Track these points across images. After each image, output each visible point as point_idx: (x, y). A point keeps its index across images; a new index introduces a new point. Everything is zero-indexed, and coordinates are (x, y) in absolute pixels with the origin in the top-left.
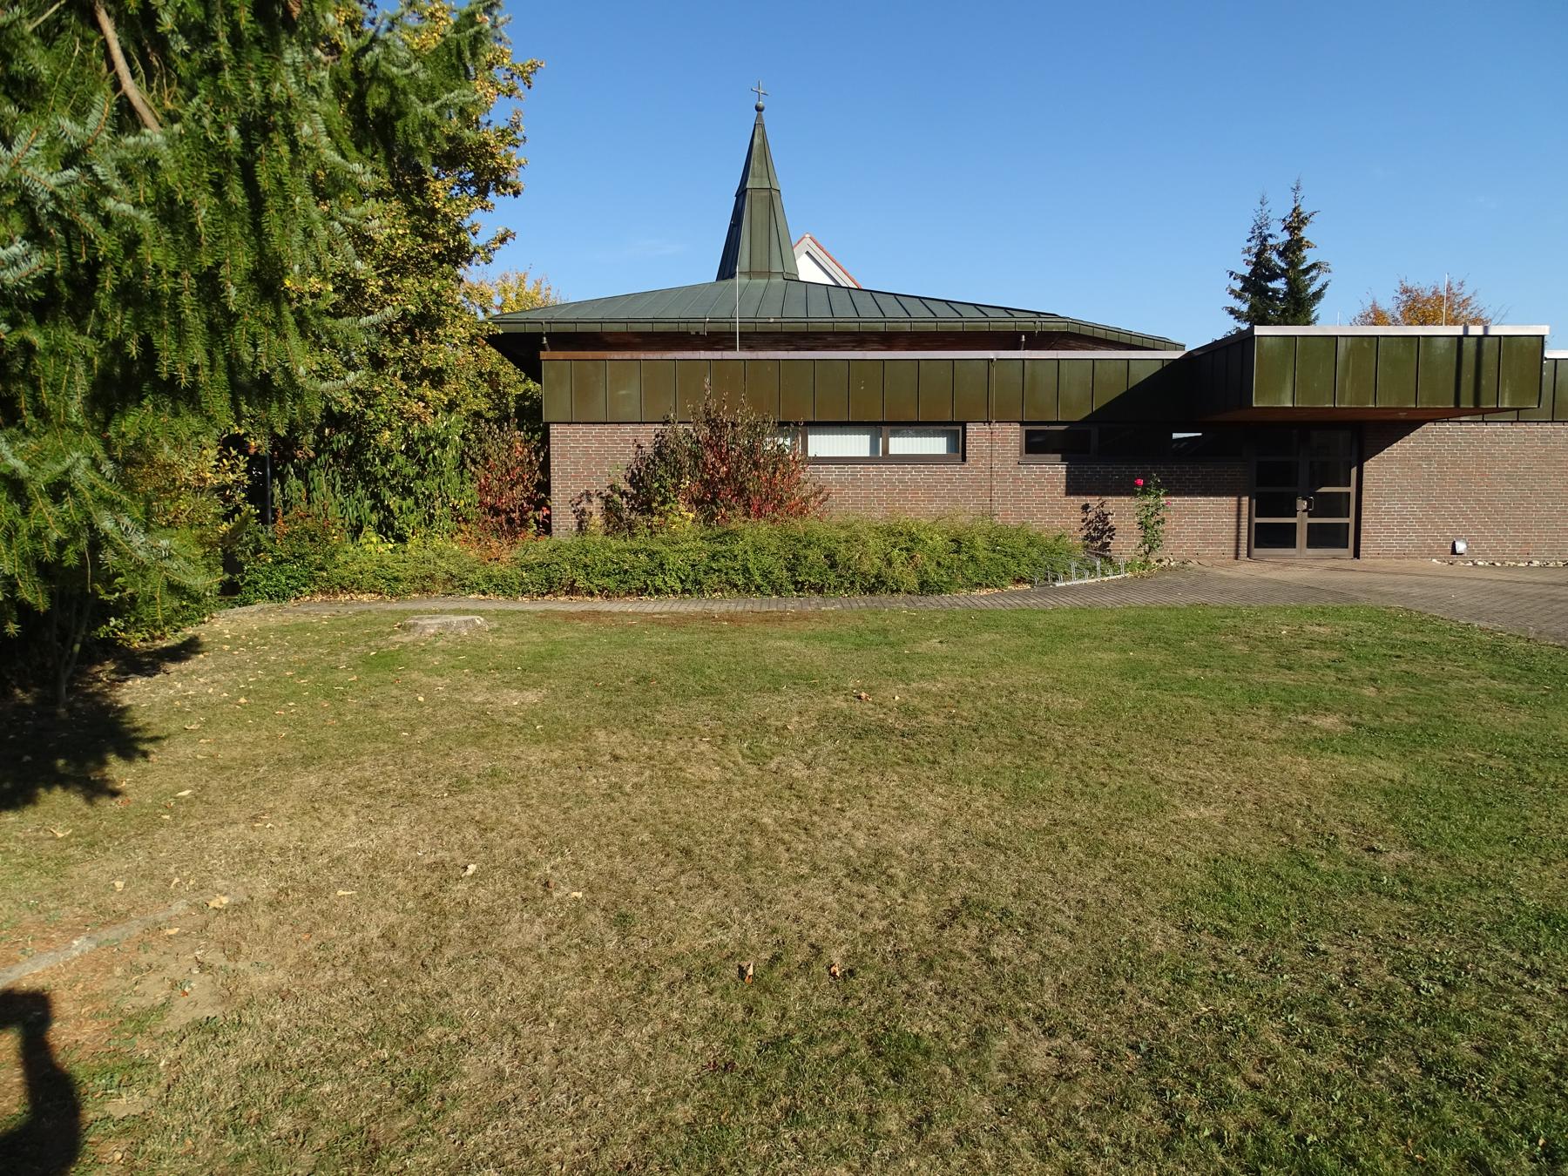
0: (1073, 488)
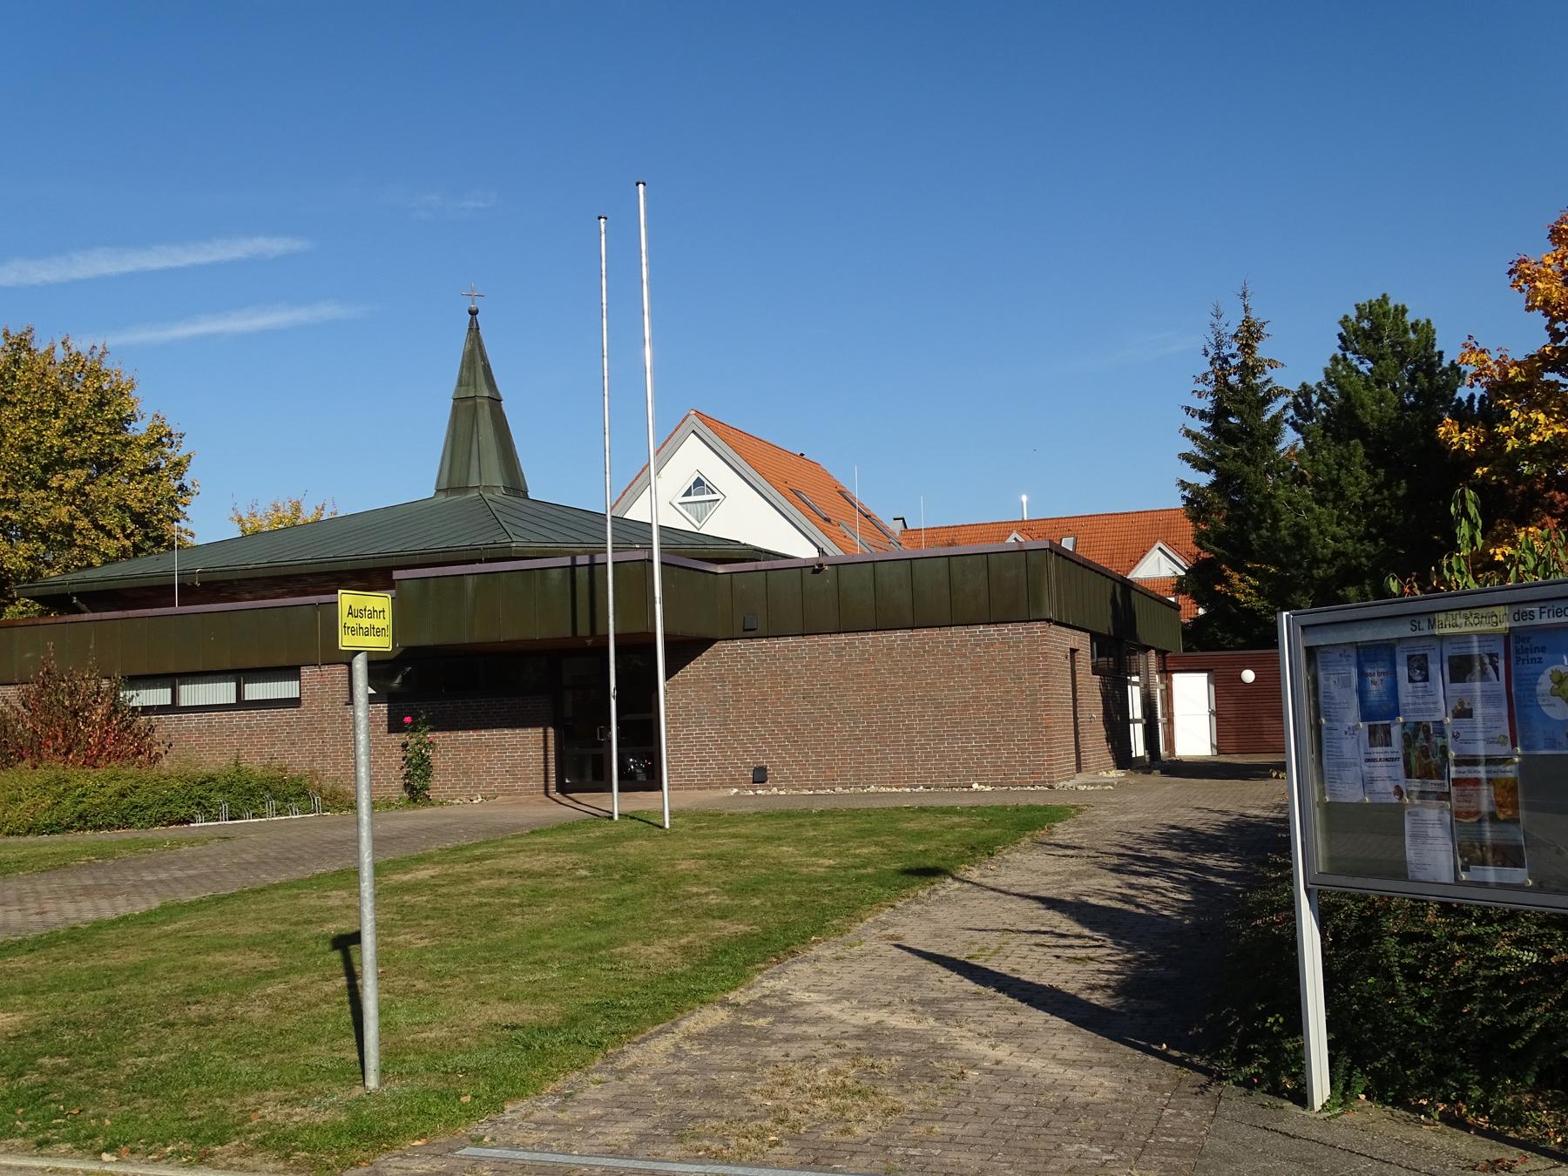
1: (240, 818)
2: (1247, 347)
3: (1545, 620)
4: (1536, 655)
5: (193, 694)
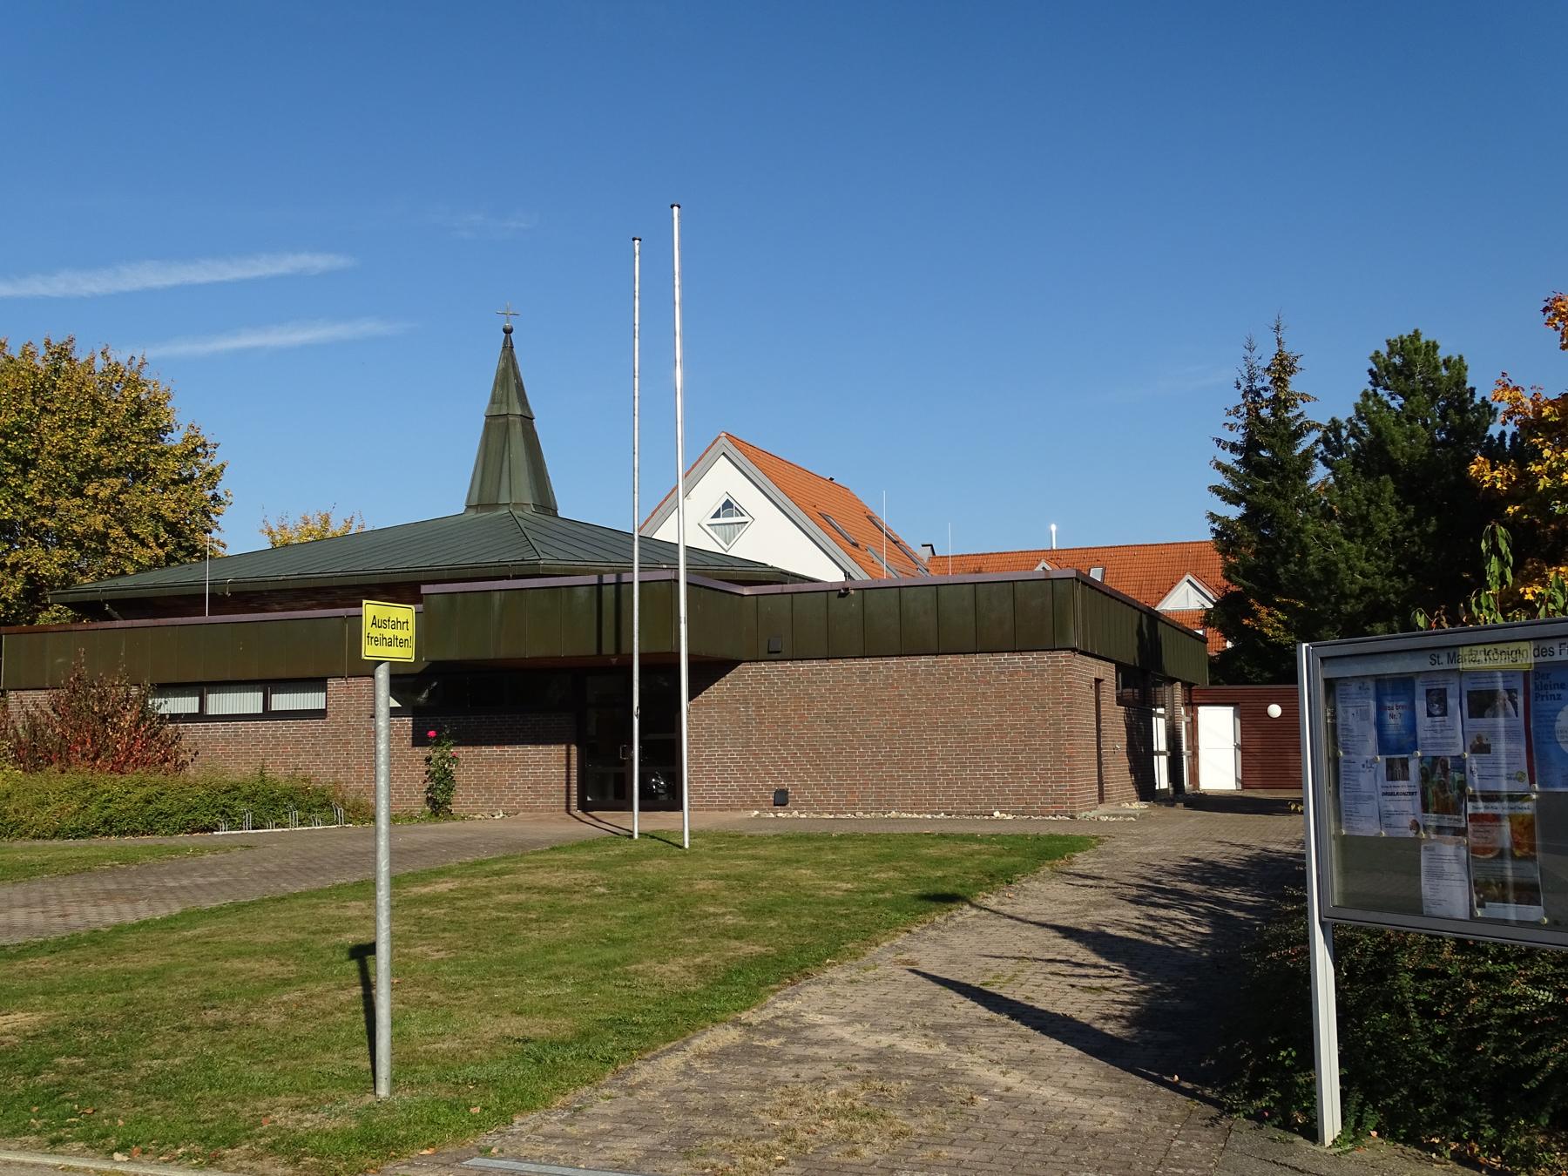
0: (419, 740)
1: (263, 827)
2: (1279, 381)
5: (221, 703)
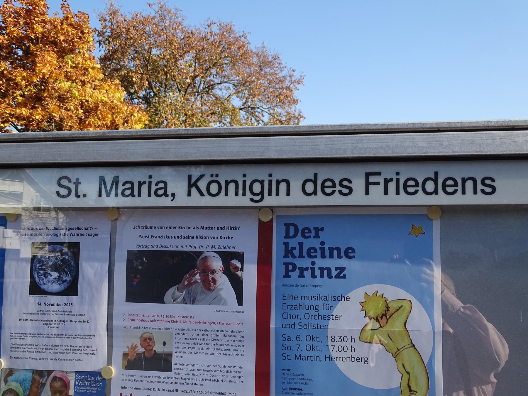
3: (377, 197)
4: (333, 263)
